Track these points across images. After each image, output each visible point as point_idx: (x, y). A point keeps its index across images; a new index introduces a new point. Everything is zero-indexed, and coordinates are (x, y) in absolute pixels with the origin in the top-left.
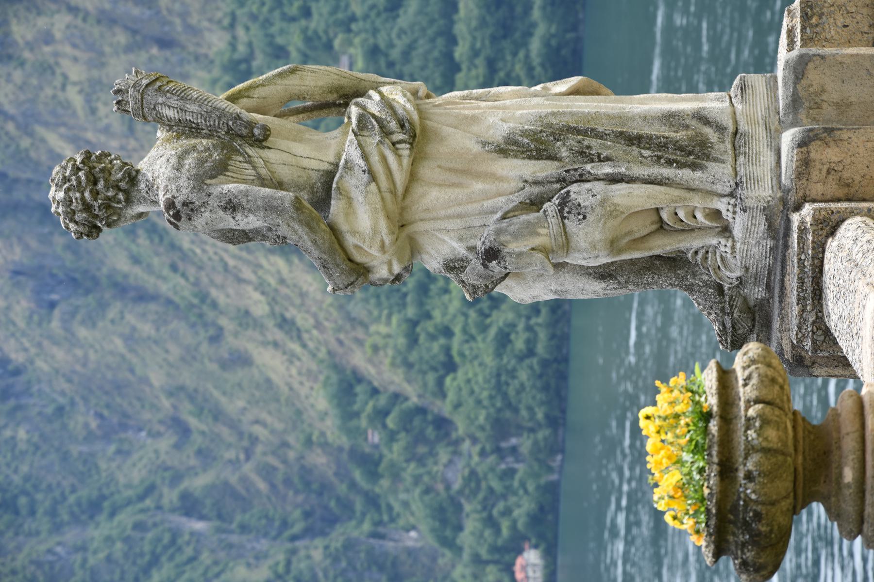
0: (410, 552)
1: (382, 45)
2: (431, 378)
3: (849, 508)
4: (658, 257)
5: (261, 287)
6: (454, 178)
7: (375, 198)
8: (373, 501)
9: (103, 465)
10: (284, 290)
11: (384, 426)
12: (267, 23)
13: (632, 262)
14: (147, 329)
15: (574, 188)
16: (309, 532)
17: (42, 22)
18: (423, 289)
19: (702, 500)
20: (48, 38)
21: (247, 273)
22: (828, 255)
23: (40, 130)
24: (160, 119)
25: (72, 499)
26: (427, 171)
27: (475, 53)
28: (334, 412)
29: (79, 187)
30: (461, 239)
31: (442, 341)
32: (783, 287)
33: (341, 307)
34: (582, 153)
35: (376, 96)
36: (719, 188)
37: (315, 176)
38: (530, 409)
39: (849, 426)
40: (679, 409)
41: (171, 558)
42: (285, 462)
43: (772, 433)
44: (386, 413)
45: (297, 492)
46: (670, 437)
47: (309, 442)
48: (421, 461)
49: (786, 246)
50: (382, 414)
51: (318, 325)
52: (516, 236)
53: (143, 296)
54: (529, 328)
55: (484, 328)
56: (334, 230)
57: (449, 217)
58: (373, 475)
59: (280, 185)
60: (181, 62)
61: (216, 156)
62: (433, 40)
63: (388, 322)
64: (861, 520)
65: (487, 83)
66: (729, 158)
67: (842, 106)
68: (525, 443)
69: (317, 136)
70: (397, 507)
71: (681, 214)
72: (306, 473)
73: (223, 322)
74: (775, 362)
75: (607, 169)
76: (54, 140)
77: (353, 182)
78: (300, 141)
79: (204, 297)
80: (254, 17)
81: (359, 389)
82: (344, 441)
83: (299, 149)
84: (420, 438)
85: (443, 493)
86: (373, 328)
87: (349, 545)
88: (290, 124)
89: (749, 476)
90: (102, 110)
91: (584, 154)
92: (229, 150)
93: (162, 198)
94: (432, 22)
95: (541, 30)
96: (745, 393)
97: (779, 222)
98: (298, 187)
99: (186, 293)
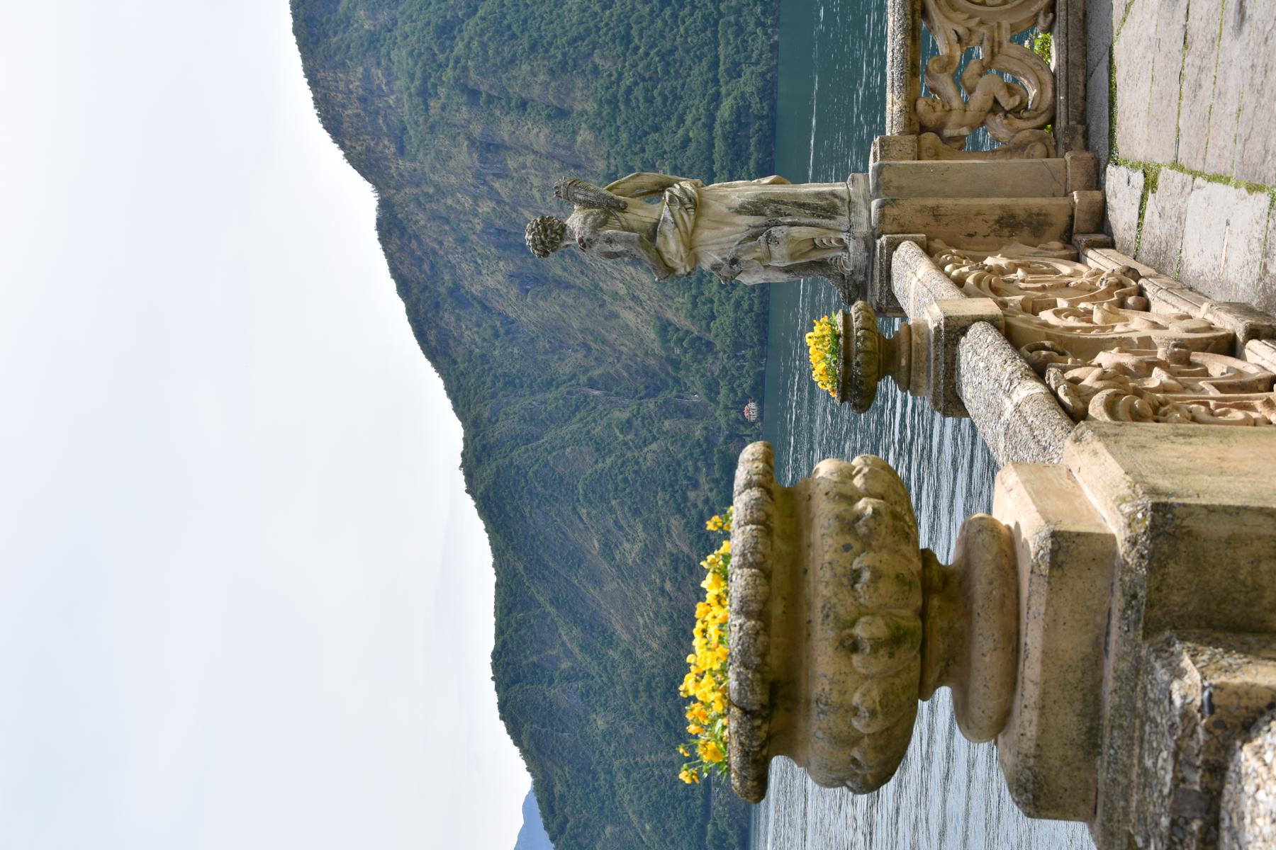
0: (695, 404)
1: (679, 165)
2: (704, 323)
3: (903, 377)
4: (814, 262)
5: (623, 281)
6: (715, 225)
7: (678, 236)
8: (677, 381)
9: (552, 365)
10: (633, 282)
11: (682, 346)
12: (624, 155)
13: (801, 264)
14: (570, 301)
15: (773, 229)
16: (648, 396)
17: (521, 159)
18: (700, 281)
19: (836, 375)
20: (524, 166)
21: (616, 275)
22: (894, 259)
23: (521, 209)
24: (576, 200)
25: (539, 380)
26: (703, 222)
27: (723, 168)
28: (658, 340)
29: (539, 233)
30: (719, 255)
31: (709, 305)
32: (872, 275)
33: (661, 290)
34: (776, 212)
35: (678, 187)
36: (842, 228)
37: (649, 225)
38: (751, 337)
39: (904, 339)
40: (824, 333)
41: (585, 407)
42: (636, 363)
43: (868, 344)
44: (683, 340)
45: (642, 377)
46: (820, 346)
47: (647, 354)
48: (699, 362)
49: (874, 255)
50: (681, 340)
51: (650, 299)
52: (745, 253)
53: (568, 286)
54: (750, 299)
55: (729, 299)
56: (658, 251)
57: (713, 244)
58: (677, 369)
59: (632, 230)
60: (584, 175)
61: (602, 217)
62: (703, 162)
63: (683, 297)
64: (909, 383)
65: (731, 179)
66: (847, 213)
67: (900, 188)
68: (748, 353)
69: (650, 206)
70: (688, 384)
71: (824, 241)
72: (646, 368)
73: (606, 298)
74: (870, 310)
75: (789, 220)
76: (527, 214)
77: (667, 228)
78: (642, 209)
79: (596, 286)
80: (618, 153)
81: (670, 329)
82: (663, 353)
83: (641, 213)
84: (699, 351)
85: (710, 377)
86: (676, 300)
87: (666, 401)
88: (637, 201)
89: (858, 364)
90: (549, 199)
91: (778, 213)
92: (608, 214)
93: (577, 237)
94: (702, 153)
95: (754, 156)
96: (856, 325)
97: (870, 243)
98: (641, 231)
99: (588, 285)
